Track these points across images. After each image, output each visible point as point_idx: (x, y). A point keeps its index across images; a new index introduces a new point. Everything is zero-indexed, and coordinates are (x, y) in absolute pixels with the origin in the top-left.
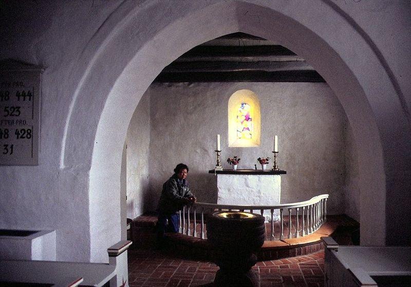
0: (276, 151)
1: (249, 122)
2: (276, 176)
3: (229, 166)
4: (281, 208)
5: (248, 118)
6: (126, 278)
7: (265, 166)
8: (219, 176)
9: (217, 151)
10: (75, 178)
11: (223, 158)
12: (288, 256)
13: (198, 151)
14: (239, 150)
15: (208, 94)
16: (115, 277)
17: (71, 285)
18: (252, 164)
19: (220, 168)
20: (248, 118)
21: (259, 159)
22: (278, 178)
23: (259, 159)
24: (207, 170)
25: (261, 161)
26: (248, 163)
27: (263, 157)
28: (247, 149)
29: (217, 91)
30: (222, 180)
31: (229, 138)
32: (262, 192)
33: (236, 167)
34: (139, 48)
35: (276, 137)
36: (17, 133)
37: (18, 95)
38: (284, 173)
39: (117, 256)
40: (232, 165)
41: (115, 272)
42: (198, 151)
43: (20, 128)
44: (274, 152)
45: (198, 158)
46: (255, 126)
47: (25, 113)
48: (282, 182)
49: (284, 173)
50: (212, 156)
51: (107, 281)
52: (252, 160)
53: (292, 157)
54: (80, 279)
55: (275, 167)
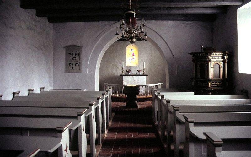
0: (144, 67)
1: (134, 56)
2: (144, 76)
3: (127, 73)
4: (145, 86)
5: (133, 55)
6: (68, 145)
7: (140, 73)
8: (123, 76)
9: (122, 68)
10: (91, 76)
11: (124, 70)
12: (148, 101)
13: (115, 68)
14: (130, 67)
15: (118, 46)
16: (99, 105)
17: (30, 156)
18: (135, 72)
19: (123, 74)
20: (133, 55)
21: (138, 71)
22: (145, 77)
23: (138, 71)
24: (119, 75)
25: (139, 71)
26: (134, 72)
27: (139, 70)
28: (134, 67)
29: (122, 44)
30: (125, 78)
31: (126, 63)
32: (139, 82)
33: (129, 73)
34: (107, 42)
35: (144, 62)
36: (75, 64)
37: (75, 54)
38: (147, 75)
39: (63, 132)
40: (128, 73)
41: (92, 112)
42: (115, 68)
43: (76, 63)
44: (144, 68)
45: (114, 70)
46: (136, 58)
47: (78, 59)
48: (147, 79)
49: (147, 75)
50: (120, 69)
51: (77, 127)
52: (135, 71)
53: (150, 70)
54: (38, 149)
55: (144, 73)
